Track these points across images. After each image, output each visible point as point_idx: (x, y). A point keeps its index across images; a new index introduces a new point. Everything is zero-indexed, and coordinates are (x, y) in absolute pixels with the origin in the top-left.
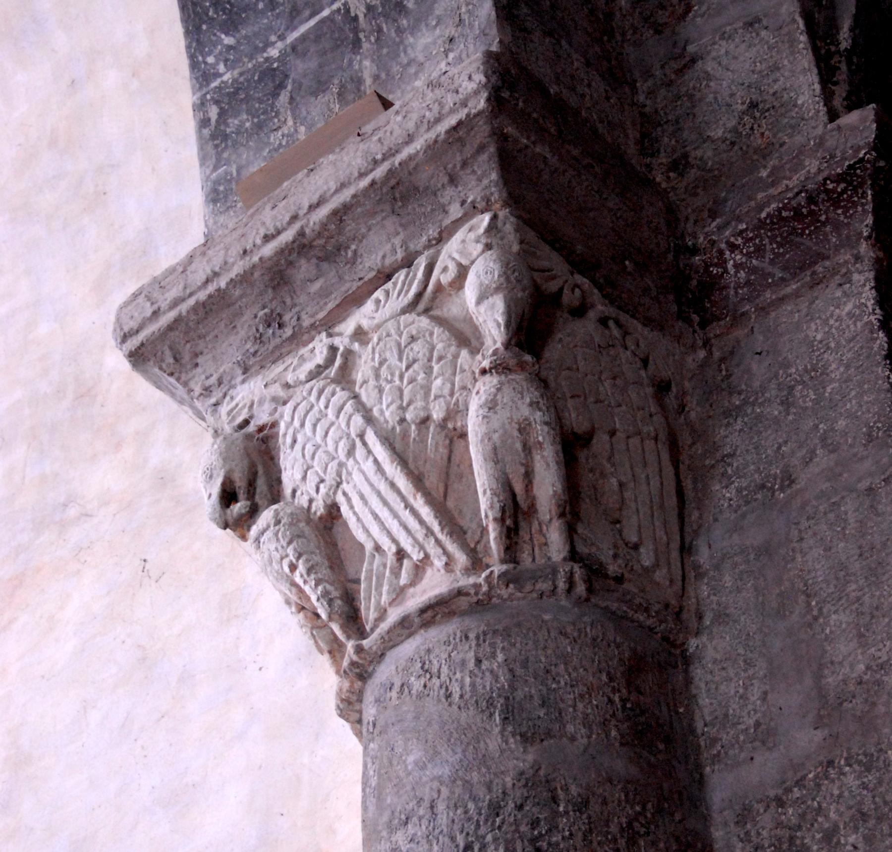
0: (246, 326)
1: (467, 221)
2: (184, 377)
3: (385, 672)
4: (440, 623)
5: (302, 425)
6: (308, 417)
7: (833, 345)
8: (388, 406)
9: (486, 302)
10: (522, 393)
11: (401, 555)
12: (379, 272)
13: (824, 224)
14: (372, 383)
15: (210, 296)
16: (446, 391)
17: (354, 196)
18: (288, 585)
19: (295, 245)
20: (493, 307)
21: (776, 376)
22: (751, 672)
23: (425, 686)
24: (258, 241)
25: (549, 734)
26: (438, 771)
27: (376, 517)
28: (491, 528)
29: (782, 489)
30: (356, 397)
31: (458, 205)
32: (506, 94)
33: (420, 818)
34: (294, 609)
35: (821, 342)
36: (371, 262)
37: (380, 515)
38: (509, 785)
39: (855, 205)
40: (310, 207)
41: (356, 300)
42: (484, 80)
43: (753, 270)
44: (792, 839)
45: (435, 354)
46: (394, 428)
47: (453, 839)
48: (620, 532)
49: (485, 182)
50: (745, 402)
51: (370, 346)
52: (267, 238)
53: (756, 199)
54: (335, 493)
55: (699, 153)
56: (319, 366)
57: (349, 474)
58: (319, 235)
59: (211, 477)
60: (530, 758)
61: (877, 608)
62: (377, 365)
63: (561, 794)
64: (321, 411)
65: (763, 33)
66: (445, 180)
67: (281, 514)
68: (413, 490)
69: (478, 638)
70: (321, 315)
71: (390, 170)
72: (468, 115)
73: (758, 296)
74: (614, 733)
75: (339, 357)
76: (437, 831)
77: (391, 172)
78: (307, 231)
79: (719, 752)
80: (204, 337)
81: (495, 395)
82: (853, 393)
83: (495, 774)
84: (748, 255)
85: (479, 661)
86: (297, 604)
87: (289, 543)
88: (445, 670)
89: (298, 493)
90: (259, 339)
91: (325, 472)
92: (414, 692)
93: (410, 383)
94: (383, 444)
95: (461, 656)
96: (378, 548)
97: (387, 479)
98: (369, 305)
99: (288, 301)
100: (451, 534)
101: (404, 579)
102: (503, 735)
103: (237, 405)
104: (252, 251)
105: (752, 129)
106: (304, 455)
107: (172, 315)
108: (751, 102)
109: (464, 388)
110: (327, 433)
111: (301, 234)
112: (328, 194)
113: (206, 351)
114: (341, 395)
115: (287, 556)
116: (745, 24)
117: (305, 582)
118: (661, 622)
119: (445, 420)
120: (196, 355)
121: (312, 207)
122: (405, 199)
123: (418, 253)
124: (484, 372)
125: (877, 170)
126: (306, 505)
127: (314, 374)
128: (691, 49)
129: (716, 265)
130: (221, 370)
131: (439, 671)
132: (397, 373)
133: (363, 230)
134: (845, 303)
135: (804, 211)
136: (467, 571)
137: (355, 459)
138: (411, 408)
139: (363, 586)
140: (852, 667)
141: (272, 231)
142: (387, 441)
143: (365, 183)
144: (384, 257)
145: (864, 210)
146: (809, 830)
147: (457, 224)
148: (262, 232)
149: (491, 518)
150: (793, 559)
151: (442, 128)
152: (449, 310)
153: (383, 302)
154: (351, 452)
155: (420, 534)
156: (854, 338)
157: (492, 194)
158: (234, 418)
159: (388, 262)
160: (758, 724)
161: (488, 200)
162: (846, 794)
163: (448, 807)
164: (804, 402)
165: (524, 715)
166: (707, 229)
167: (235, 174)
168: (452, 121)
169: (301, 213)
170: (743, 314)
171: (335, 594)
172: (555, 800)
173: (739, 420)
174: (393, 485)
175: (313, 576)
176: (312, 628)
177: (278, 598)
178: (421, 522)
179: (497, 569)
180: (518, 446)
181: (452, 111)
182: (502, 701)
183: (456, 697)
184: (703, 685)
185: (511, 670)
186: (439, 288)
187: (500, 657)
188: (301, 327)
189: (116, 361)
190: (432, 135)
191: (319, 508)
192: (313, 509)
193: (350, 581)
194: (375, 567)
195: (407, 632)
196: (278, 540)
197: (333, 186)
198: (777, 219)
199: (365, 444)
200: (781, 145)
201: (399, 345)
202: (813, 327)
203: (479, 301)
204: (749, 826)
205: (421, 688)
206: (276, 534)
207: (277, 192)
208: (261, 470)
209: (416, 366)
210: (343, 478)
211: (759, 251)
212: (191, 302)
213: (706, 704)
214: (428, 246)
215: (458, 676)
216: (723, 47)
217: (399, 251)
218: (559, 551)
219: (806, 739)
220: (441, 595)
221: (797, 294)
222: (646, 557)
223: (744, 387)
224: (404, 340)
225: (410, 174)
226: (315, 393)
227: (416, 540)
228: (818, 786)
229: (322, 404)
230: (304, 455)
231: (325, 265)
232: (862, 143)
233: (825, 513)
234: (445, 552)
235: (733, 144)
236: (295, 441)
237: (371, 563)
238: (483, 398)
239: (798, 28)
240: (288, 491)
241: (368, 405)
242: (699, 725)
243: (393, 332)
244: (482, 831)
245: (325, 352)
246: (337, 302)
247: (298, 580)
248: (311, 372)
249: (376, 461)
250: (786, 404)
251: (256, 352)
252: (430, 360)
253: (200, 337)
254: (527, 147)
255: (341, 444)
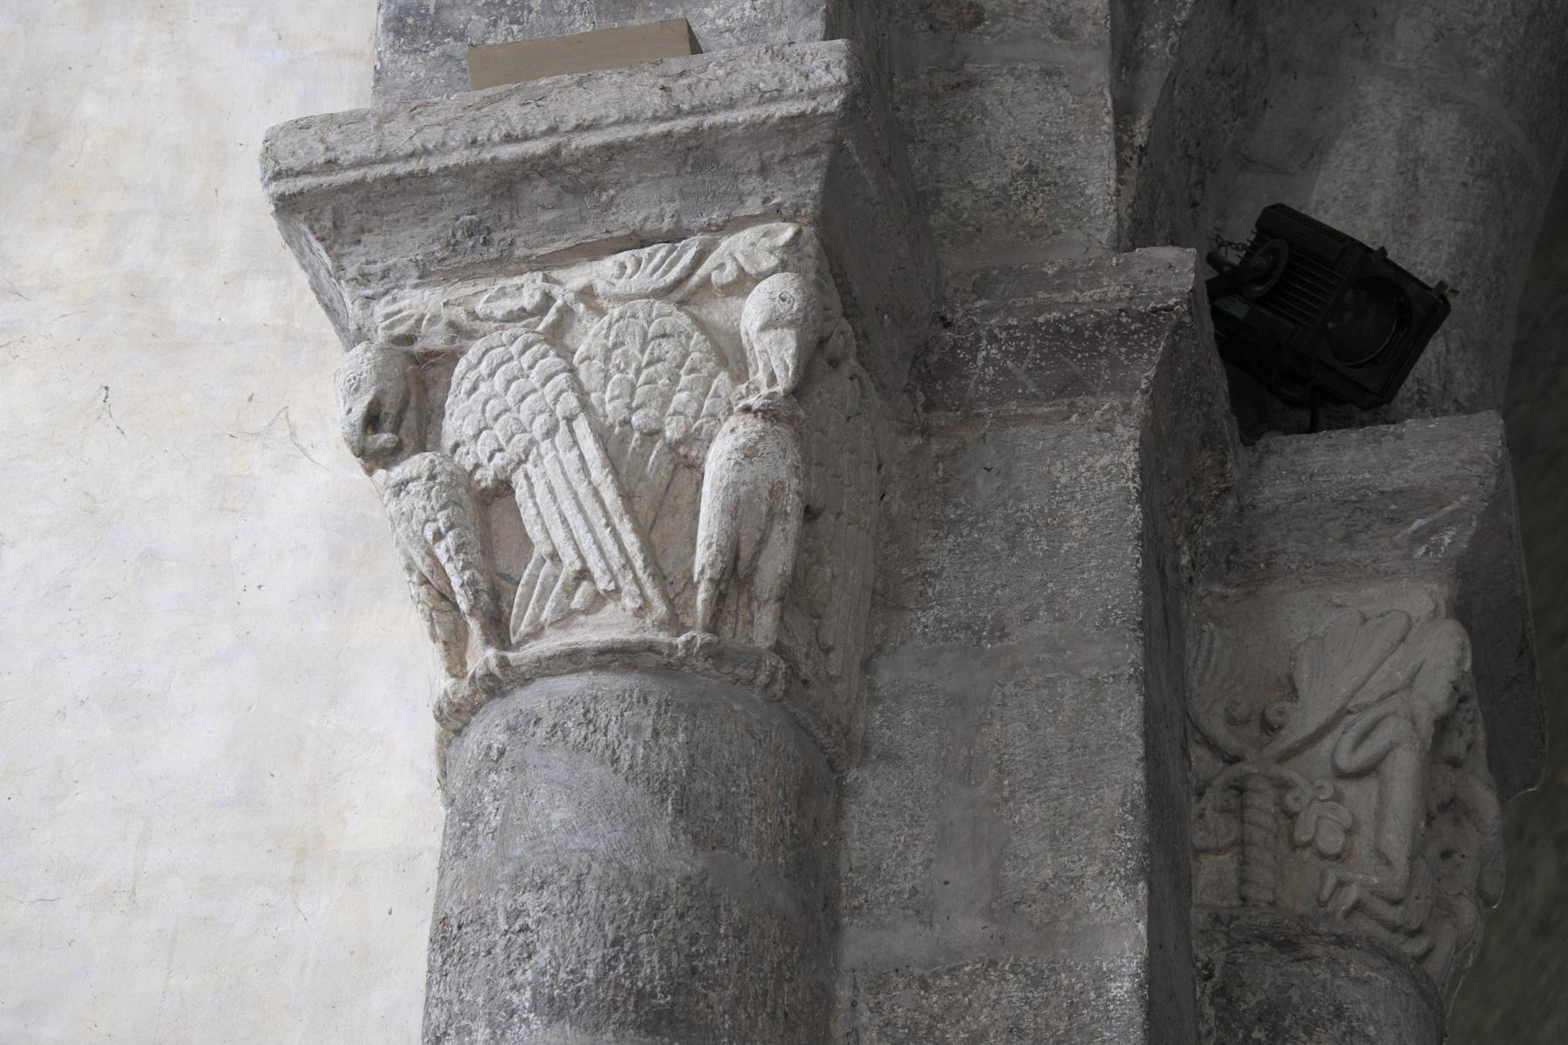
0: (440, 224)
1: (764, 222)
2: (336, 248)
3: (528, 699)
4: (615, 671)
5: (492, 374)
6: (503, 368)
7: (1079, 497)
8: (612, 399)
9: (773, 332)
10: (784, 451)
11: (584, 574)
12: (634, 233)
13: (1101, 355)
14: (597, 363)
15: (411, 175)
16: (690, 411)
17: (639, 139)
18: (423, 552)
19: (542, 162)
20: (781, 342)
21: (1005, 504)
22: (916, 831)
23: (585, 739)
24: (496, 137)
25: (721, 843)
26: (590, 843)
27: (564, 521)
28: (702, 588)
29: (990, 638)
30: (572, 370)
31: (759, 201)
32: (861, 103)
33: (562, 889)
34: (415, 579)
35: (1065, 487)
36: (628, 217)
37: (570, 520)
38: (673, 887)
39: (1142, 350)
40: (578, 126)
41: (594, 251)
42: (845, 79)
43: (1006, 372)
44: (930, 1028)
45: (688, 363)
46: (612, 426)
47: (600, 926)
48: (817, 629)
49: (802, 189)
50: (961, 520)
51: (606, 318)
52: (509, 139)
53: (1035, 297)
54: (513, 471)
55: (955, 197)
56: (523, 309)
57: (540, 456)
58: (577, 163)
59: (357, 390)
60: (699, 864)
61: (1078, 816)
62: (610, 344)
63: (723, 913)
64: (521, 369)
65: (1062, 91)
66: (756, 166)
67: (438, 469)
68: (621, 510)
69: (659, 706)
70: (542, 251)
71: (696, 129)
72: (815, 110)
73: (1002, 403)
74: (780, 860)
75: (553, 310)
76: (581, 911)
77: (696, 131)
78: (564, 152)
79: (861, 905)
80: (383, 215)
81: (756, 443)
82: (1094, 562)
83: (659, 870)
84: (1006, 353)
85: (656, 734)
86: (421, 574)
87: (443, 507)
88: (614, 729)
89: (462, 450)
90: (453, 246)
91: (508, 441)
92: (571, 739)
93: (646, 383)
94: (596, 441)
95: (636, 719)
96: (554, 556)
97: (590, 483)
98: (609, 264)
99: (506, 217)
100: (653, 575)
101: (577, 601)
102: (673, 829)
103: (400, 311)
104: (483, 145)
105: (1025, 197)
106: (484, 411)
107: (352, 175)
108: (1030, 166)
109: (713, 416)
110: (524, 398)
111: (556, 151)
112: (605, 122)
113: (377, 231)
114: (552, 361)
115: (435, 520)
116: (1042, 70)
117: (450, 559)
118: (836, 744)
119: (679, 443)
120: (363, 231)
121: (579, 128)
122: (698, 167)
123: (691, 233)
124: (747, 409)
125: (1180, 324)
126: (469, 468)
127: (514, 317)
128: (970, 68)
129: (965, 349)
130: (391, 262)
131: (606, 728)
132: (634, 365)
133: (632, 179)
134: (1101, 454)
135: (1087, 333)
136: (661, 625)
137: (553, 443)
138: (641, 413)
139: (520, 590)
140: (1038, 866)
141: (518, 132)
142: (602, 436)
143: (656, 129)
144: (646, 219)
145: (1149, 360)
146: (953, 1025)
147: (751, 221)
148: (504, 129)
149: (707, 576)
150: (990, 724)
151: (779, 110)
152: (709, 313)
153: (629, 271)
154: (550, 433)
155: (616, 562)
156: (1106, 498)
157: (804, 205)
158: (392, 326)
159: (649, 226)
160: (914, 892)
161: (798, 210)
162: (1004, 1002)
163: (599, 888)
164: (1034, 549)
165: (699, 813)
166: (968, 306)
167: (432, 11)
168: (794, 108)
169: (563, 128)
170: (978, 415)
171: (483, 586)
172: (716, 917)
173: (951, 539)
174: (596, 493)
175: (462, 556)
176: (432, 609)
177: (397, 561)
178: (622, 550)
179: (701, 637)
180: (764, 509)
181: (794, 97)
182: (677, 788)
183: (625, 764)
184: (856, 825)
185: (691, 757)
186: (706, 282)
187: (681, 737)
188: (512, 254)
189: (250, 193)
190: (760, 113)
191: (486, 477)
192: (477, 476)
193: (498, 574)
194: (542, 575)
195: (571, 666)
196: (429, 498)
197: (614, 115)
198: (1054, 329)
199: (571, 431)
200: (1057, 233)
201: (645, 333)
202: (1059, 466)
203: (765, 328)
204: (881, 997)
205: (580, 739)
206: (429, 490)
207: (531, 84)
208: (413, 402)
209: (659, 366)
210: (531, 458)
211: (1019, 355)
212: (385, 170)
213: (855, 851)
214: (703, 230)
215: (630, 741)
216: (1008, 85)
217: (667, 220)
218: (766, 637)
219: (969, 928)
220: (628, 642)
221: (1045, 419)
222: (835, 664)
223: (962, 500)
224: (652, 330)
225: (717, 142)
226: (519, 344)
227: (609, 569)
228: (975, 983)
229: (526, 360)
230: (484, 411)
231: (568, 197)
232: (1175, 289)
233: (1037, 687)
234: (642, 595)
235: (998, 204)
236: (474, 388)
237: (538, 568)
238: (742, 441)
239: (1105, 105)
240: (448, 443)
241: (587, 387)
242: (844, 869)
243: (641, 314)
244: (636, 929)
245: (537, 297)
246: (567, 245)
247: (440, 552)
248: (511, 312)
249: (581, 456)
250: (1013, 541)
251: (444, 259)
252: (679, 366)
253: (376, 213)
254: (856, 166)
255: (540, 419)
